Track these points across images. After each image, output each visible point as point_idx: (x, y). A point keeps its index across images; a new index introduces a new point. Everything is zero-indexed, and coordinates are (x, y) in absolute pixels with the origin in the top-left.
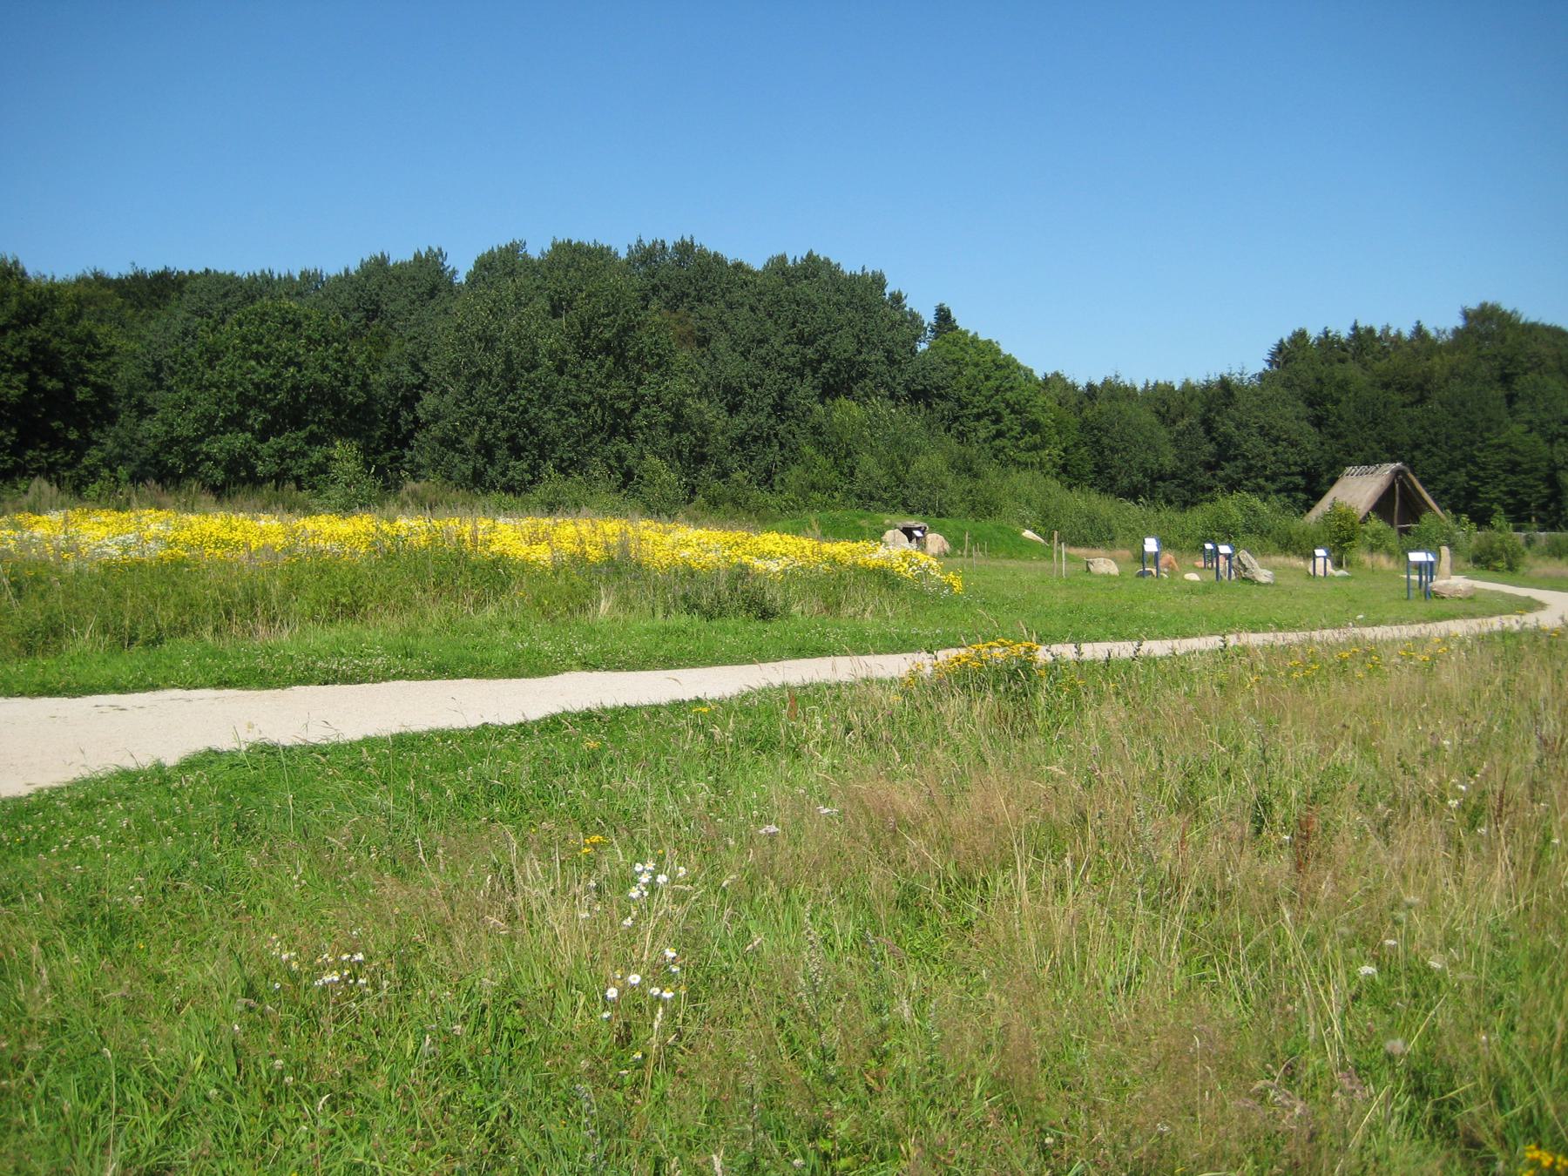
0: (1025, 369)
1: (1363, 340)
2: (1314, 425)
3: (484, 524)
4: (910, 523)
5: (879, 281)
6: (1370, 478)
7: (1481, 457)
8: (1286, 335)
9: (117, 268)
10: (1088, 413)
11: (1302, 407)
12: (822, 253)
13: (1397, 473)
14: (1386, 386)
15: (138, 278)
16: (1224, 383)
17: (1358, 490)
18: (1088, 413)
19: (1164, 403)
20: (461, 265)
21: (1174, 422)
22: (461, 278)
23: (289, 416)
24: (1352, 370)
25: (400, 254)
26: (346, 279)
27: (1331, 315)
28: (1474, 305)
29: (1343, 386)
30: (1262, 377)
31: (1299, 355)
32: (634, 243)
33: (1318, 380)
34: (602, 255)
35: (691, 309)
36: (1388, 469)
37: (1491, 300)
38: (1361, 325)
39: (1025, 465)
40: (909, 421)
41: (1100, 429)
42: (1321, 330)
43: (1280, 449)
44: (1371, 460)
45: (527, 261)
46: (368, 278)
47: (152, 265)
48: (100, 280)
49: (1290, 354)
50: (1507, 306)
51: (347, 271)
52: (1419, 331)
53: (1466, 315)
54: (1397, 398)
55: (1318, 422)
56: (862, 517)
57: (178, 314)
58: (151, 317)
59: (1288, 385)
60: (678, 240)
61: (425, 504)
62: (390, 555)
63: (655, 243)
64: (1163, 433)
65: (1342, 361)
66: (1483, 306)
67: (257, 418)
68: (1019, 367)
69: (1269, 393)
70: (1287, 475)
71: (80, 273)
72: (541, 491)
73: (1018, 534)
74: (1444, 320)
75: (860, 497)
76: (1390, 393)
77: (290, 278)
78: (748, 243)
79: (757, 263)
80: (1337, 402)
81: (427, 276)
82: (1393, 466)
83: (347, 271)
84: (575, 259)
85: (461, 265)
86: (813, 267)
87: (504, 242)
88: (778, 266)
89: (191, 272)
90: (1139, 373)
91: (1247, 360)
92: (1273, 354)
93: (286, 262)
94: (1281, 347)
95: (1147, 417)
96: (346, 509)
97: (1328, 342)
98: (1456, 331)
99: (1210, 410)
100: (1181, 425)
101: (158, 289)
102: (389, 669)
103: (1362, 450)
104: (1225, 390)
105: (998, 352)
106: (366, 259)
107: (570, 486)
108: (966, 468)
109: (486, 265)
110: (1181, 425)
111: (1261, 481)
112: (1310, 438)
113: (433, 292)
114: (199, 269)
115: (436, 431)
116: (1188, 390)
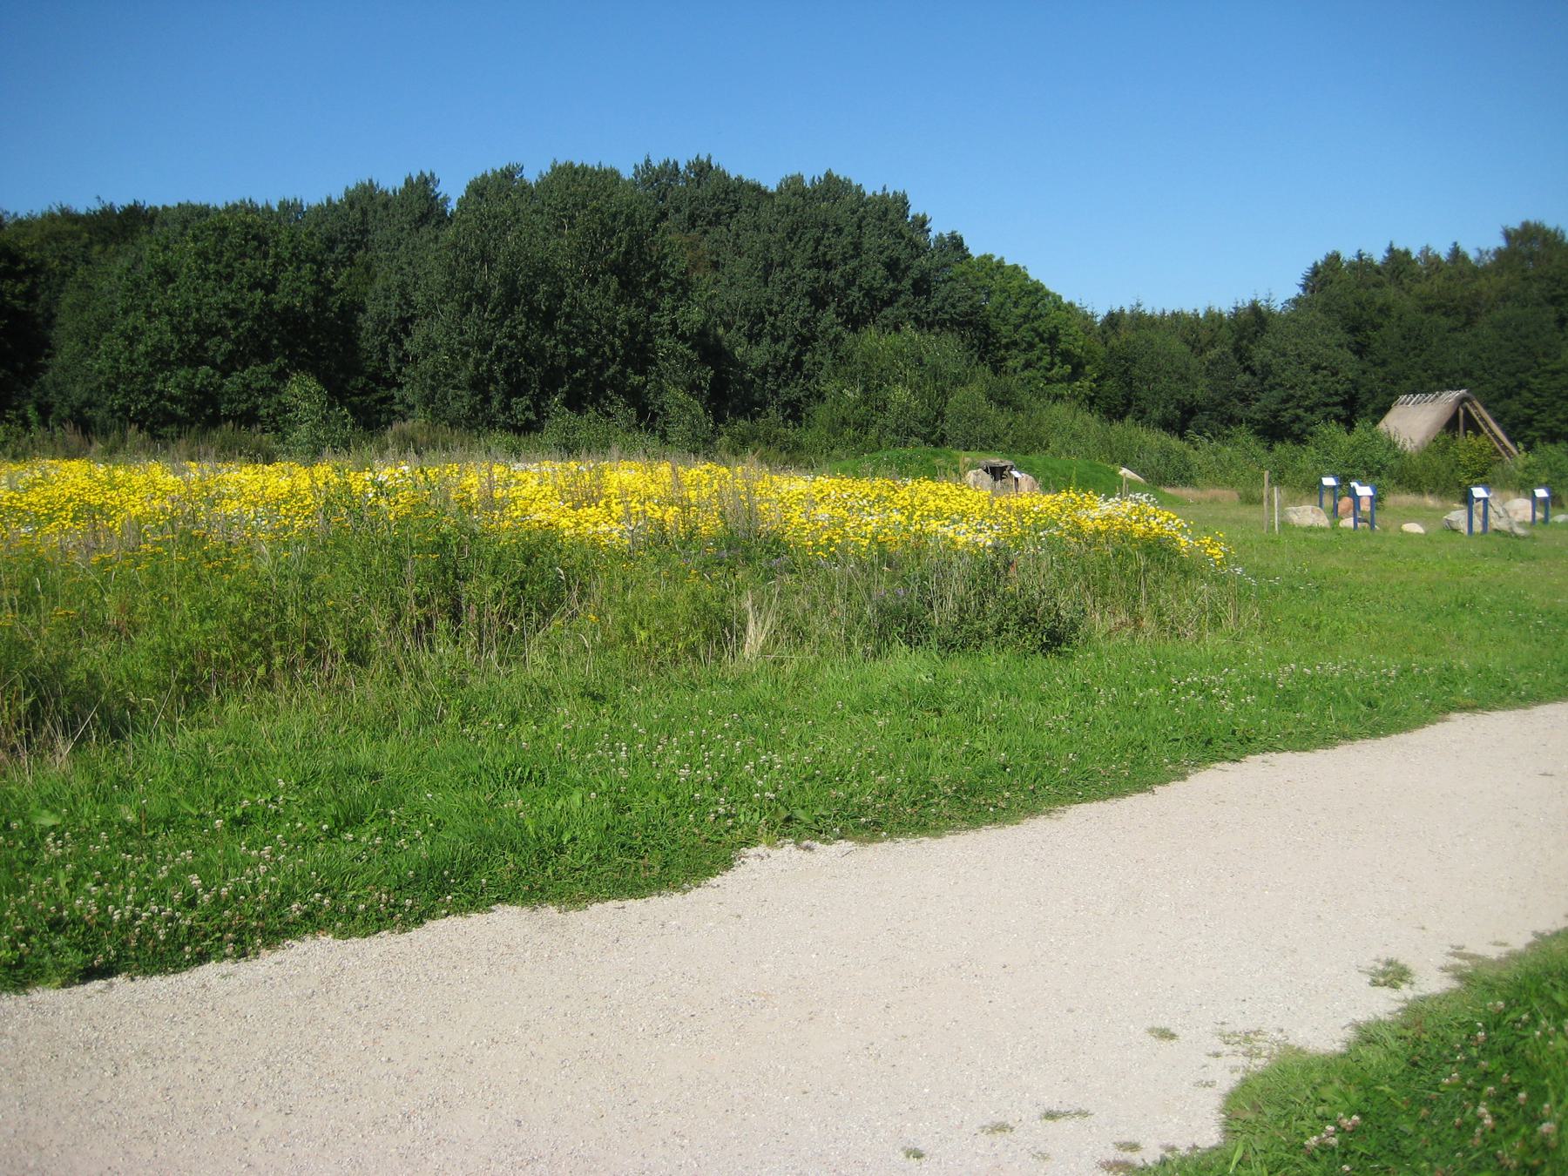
0: (1054, 295)
1: (1398, 261)
2: (1355, 352)
3: (498, 471)
4: (996, 460)
5: (902, 202)
6: (1429, 406)
7: (1535, 383)
8: (1320, 258)
9: (84, 203)
10: (1113, 342)
11: (1341, 335)
12: (841, 172)
13: (1462, 400)
14: (1429, 310)
15: (108, 213)
16: (1254, 308)
17: (1413, 422)
18: (1113, 342)
19: (1193, 331)
20: (452, 190)
21: (1202, 351)
22: (453, 206)
23: (254, 349)
24: (1391, 293)
25: (391, 181)
26: (330, 208)
27: (1366, 239)
28: (1516, 225)
29: (1385, 310)
30: (1296, 302)
31: (1336, 279)
32: (641, 162)
33: (1359, 304)
34: (609, 178)
35: (706, 232)
36: (1451, 397)
37: (1533, 219)
38: (1395, 247)
39: (1058, 397)
40: (946, 349)
41: (1126, 360)
42: (1355, 253)
43: (1319, 377)
44: (1422, 387)
45: (525, 187)
46: (352, 206)
47: (121, 200)
48: (68, 216)
49: (1325, 278)
50: (1550, 224)
51: (329, 200)
52: (1457, 254)
53: (1508, 235)
54: (1445, 322)
55: (1360, 350)
56: (936, 455)
57: (147, 245)
58: (118, 252)
59: (1327, 309)
60: (693, 158)
61: (412, 446)
62: (345, 531)
63: (667, 163)
64: (1194, 362)
65: (1378, 285)
66: (1526, 225)
67: (219, 348)
68: (1048, 294)
69: (1303, 320)
70: (1326, 405)
71: (46, 209)
72: (550, 435)
73: (1114, 473)
74: (1481, 239)
75: (896, 431)
76: (1435, 317)
77: (268, 209)
78: (763, 160)
79: (771, 184)
80: (1376, 327)
81: (421, 201)
82: (1456, 394)
83: (329, 200)
84: (578, 188)
85: (452, 190)
86: (833, 188)
87: (500, 165)
88: (793, 186)
89: (164, 207)
90: (1158, 302)
91: (1280, 287)
92: (1307, 278)
93: (268, 193)
94: (1316, 271)
95: (1177, 346)
96: (314, 454)
97: (1362, 265)
98: (1499, 253)
99: (1241, 338)
100: (1212, 353)
101: (124, 225)
102: (288, 895)
103: (1408, 378)
104: (1255, 321)
105: (1026, 277)
106: (352, 187)
107: (585, 424)
108: (1004, 401)
109: (478, 190)
110: (1212, 353)
111: (1300, 412)
112: (1350, 366)
113: (424, 219)
114: (172, 203)
115: (426, 365)
116: (1214, 318)
